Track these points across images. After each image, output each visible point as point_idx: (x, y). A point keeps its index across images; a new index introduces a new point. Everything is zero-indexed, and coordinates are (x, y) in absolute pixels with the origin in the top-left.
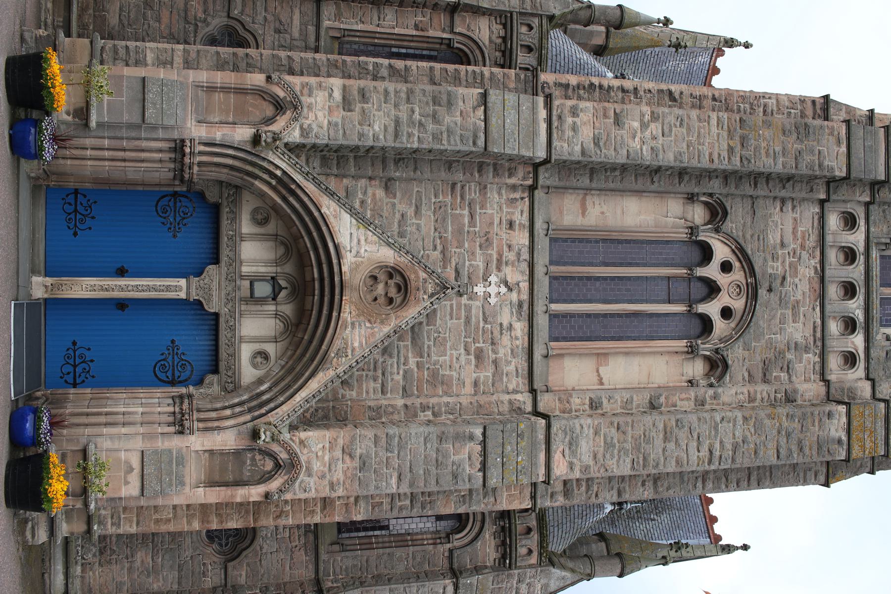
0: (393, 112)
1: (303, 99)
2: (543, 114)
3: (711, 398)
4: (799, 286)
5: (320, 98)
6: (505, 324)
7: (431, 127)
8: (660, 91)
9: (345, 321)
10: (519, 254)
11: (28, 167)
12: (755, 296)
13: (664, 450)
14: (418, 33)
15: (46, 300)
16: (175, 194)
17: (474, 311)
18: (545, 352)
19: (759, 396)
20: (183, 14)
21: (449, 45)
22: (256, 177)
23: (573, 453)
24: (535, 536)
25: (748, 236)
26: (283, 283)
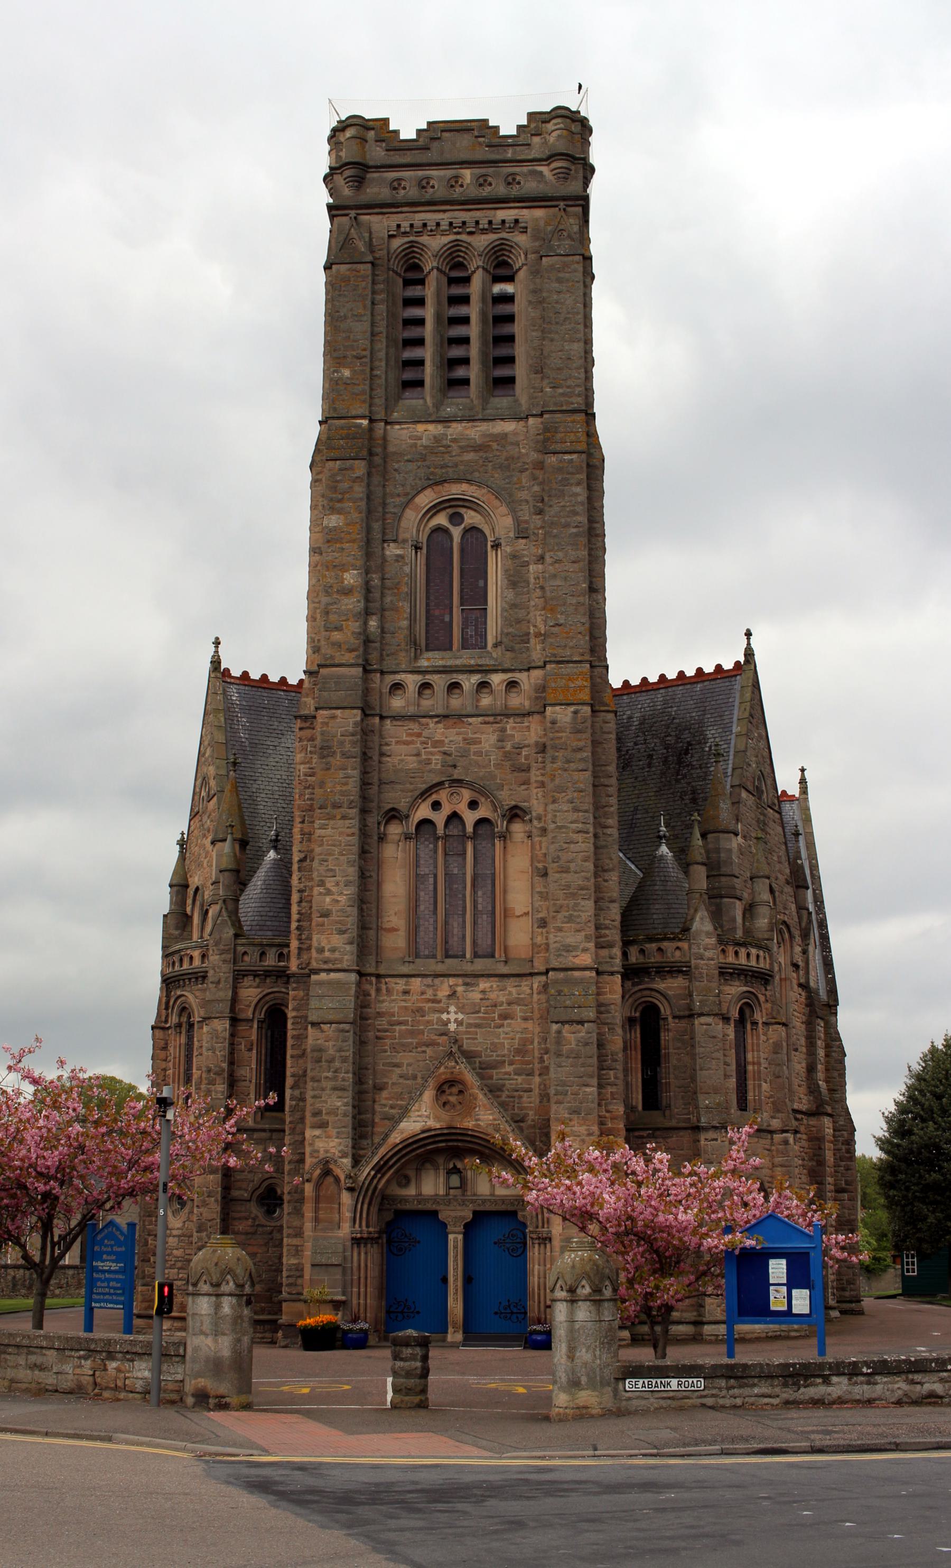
0: (328, 1092)
1: (321, 1157)
2: (323, 976)
3: (540, 822)
4: (451, 739)
5: (320, 1145)
6: (480, 996)
7: (337, 1064)
8: (300, 869)
9: (474, 1125)
10: (428, 986)
11: (372, 1340)
12: (459, 781)
13: (576, 872)
14: (255, 1048)
15: (464, 1333)
16: (389, 1242)
17: (471, 1021)
18: (502, 964)
19: (540, 778)
20: (249, 1236)
21: (262, 1022)
22: (376, 1187)
23: (575, 948)
24: (665, 945)
25: (412, 787)
26: (451, 1166)
